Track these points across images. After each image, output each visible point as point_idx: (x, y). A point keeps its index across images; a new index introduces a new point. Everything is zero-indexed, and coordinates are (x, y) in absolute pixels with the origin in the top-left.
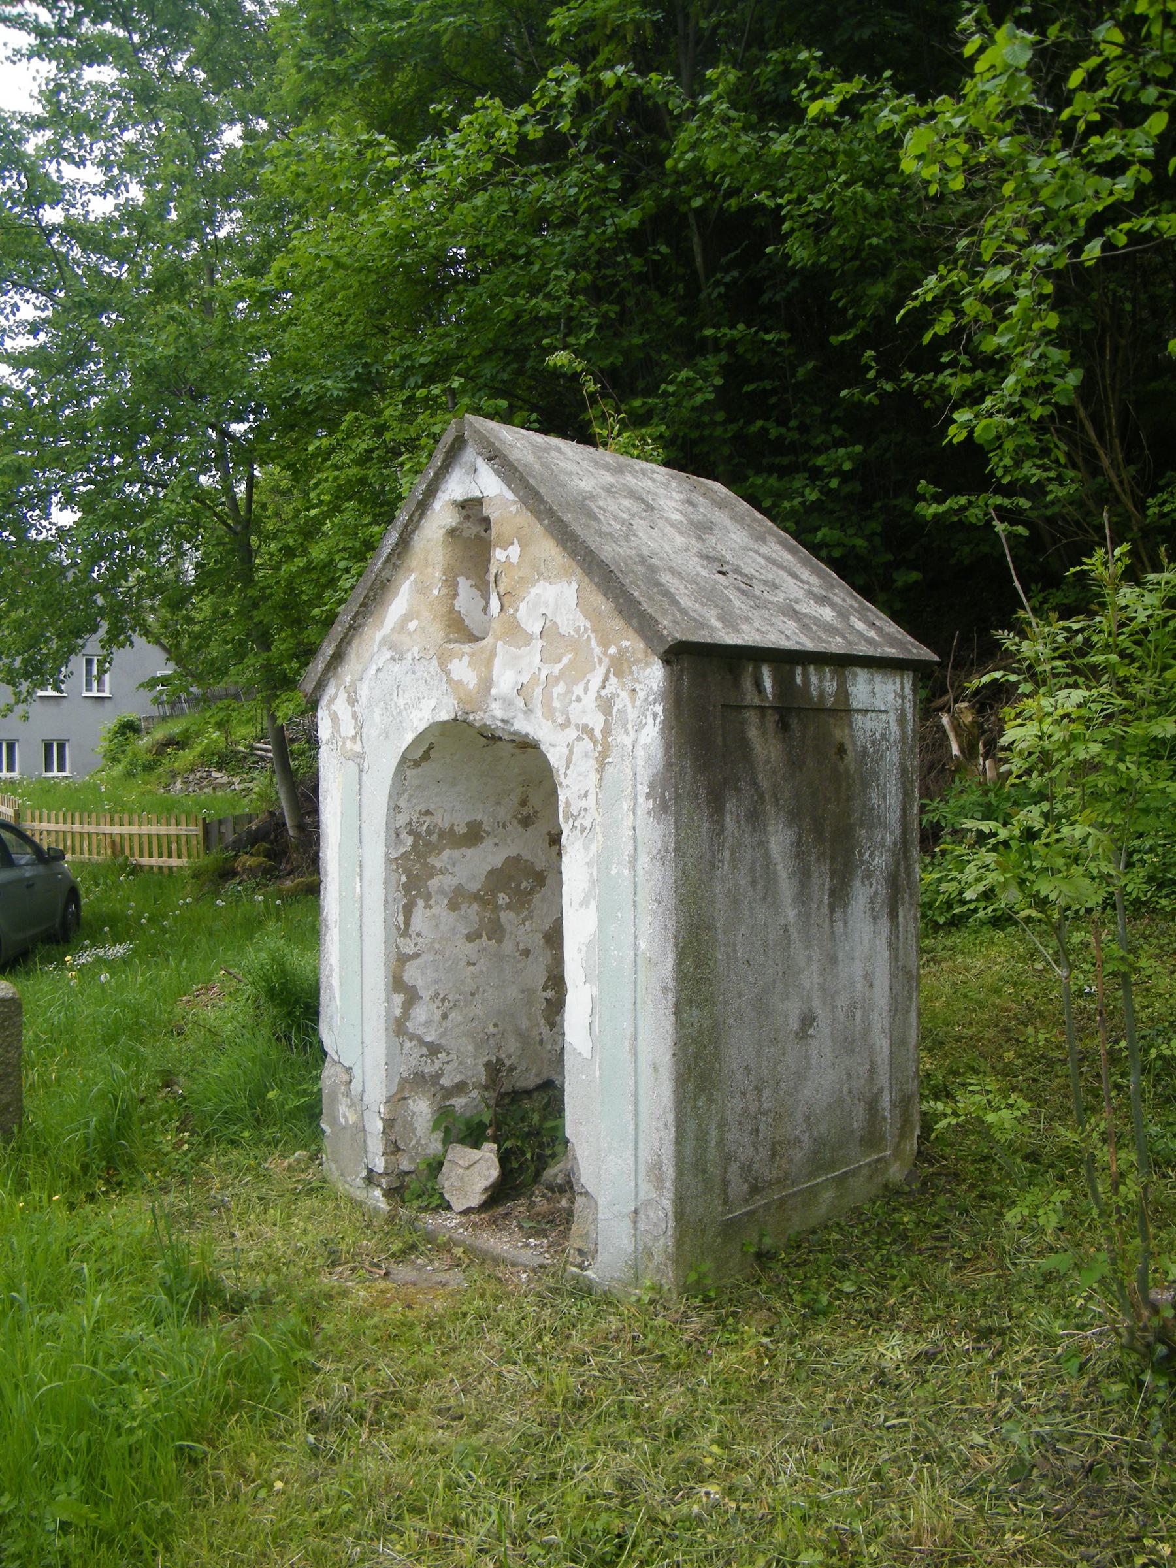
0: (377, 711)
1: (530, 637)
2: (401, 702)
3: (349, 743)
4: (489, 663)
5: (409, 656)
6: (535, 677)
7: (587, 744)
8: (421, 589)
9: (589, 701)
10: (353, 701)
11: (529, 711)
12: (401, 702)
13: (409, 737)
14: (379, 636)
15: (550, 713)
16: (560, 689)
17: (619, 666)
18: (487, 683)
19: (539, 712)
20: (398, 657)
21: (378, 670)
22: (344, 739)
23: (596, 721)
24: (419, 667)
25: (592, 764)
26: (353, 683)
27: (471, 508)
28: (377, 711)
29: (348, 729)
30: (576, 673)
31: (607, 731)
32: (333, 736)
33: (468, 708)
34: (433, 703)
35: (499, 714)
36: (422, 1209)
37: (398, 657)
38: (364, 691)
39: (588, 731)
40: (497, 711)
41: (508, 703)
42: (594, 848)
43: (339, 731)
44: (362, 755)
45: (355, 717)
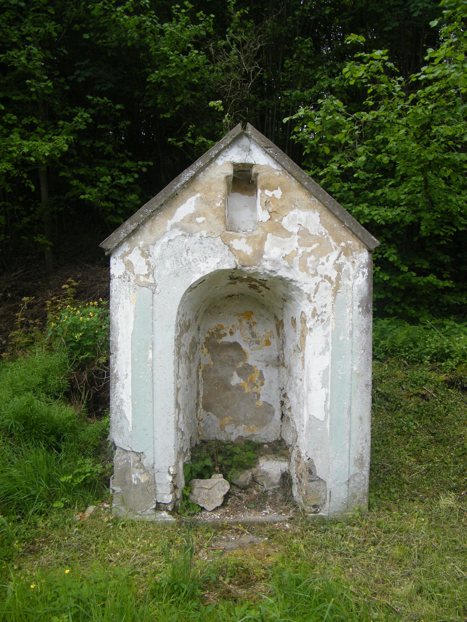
0: (168, 264)
1: (290, 234)
9: (330, 265)
21: (170, 240)
22: (138, 276)
23: (333, 275)
24: (206, 242)
26: (146, 246)
30: (323, 251)
33: (246, 263)
38: (156, 251)
40: (268, 266)
42: (330, 329)
44: (155, 285)
45: (148, 264)
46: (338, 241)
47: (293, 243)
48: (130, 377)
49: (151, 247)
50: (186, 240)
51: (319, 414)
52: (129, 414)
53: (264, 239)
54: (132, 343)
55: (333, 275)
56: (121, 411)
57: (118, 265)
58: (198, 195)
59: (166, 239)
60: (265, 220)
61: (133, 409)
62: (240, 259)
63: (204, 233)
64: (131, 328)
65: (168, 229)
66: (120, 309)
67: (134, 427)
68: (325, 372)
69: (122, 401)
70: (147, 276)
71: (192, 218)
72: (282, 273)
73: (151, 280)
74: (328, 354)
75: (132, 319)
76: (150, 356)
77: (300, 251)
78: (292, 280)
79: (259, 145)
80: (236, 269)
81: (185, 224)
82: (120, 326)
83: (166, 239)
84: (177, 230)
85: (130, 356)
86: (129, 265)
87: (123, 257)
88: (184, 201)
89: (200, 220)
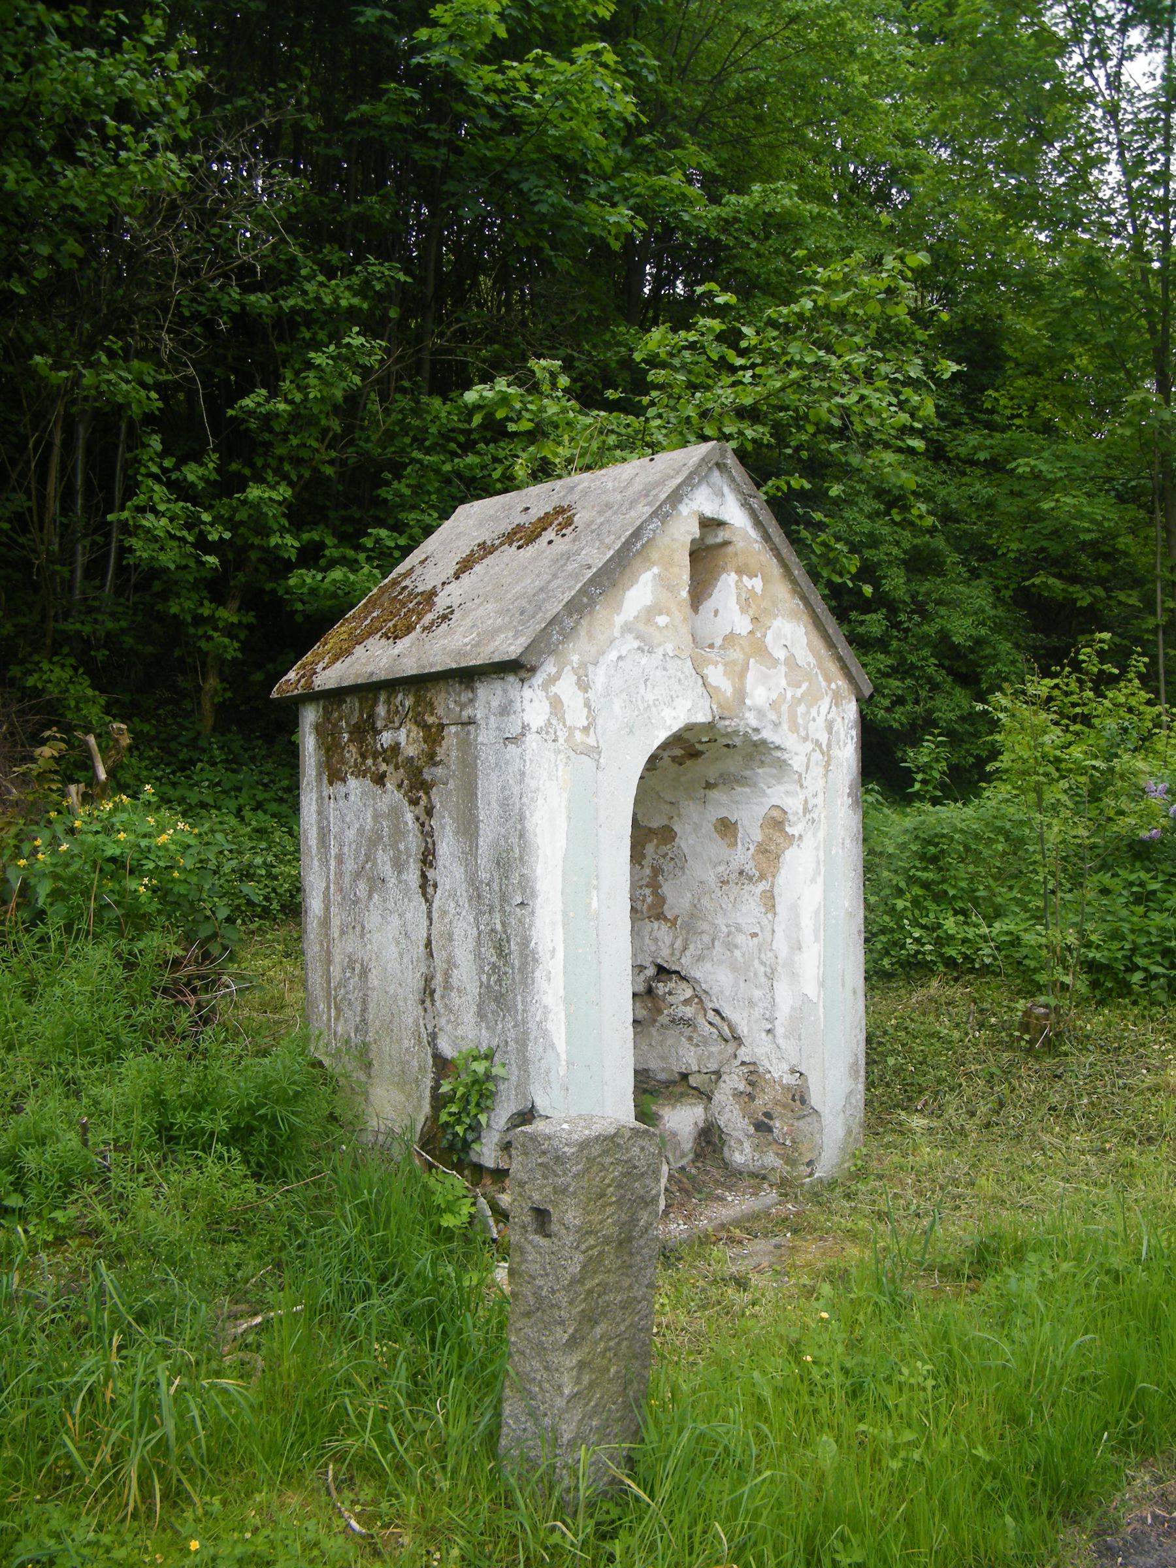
0: (617, 706)
1: (777, 661)
2: (650, 697)
3: (579, 736)
4: (742, 674)
5: (660, 651)
6: (782, 697)
7: (817, 756)
8: (665, 583)
9: (821, 721)
10: (583, 685)
11: (777, 725)
12: (650, 697)
13: (661, 736)
14: (619, 620)
15: (794, 727)
16: (801, 709)
17: (837, 699)
18: (741, 694)
19: (785, 726)
20: (647, 648)
21: (620, 658)
22: (571, 730)
23: (823, 738)
24: (672, 665)
25: (821, 770)
26: (583, 665)
27: (709, 524)
28: (617, 706)
29: (576, 716)
30: (811, 699)
31: (829, 746)
32: (549, 723)
33: (726, 714)
34: (689, 705)
35: (754, 723)
36: (82, 215)
37: (647, 648)
38: (599, 677)
39: (818, 744)
40: (752, 720)
41: (760, 713)
42: (821, 834)
43: (562, 720)
44: (597, 750)
45: (587, 705)
46: (829, 681)
47: (780, 677)
48: (560, 954)
49: (591, 668)
50: (644, 661)
51: (811, 988)
52: (559, 1036)
53: (745, 668)
54: (565, 879)
55: (823, 738)
56: (545, 1034)
57: (536, 703)
58: (655, 570)
59: (613, 655)
60: (744, 633)
61: (569, 1024)
62: (720, 706)
63: (669, 648)
64: (562, 843)
65: (617, 633)
66: (540, 802)
67: (570, 1063)
68: (817, 913)
69: (546, 1010)
70: (586, 729)
71: (651, 612)
72: (767, 734)
73: (591, 741)
74: (820, 880)
75: (564, 826)
76: (595, 904)
77: (789, 695)
78: (778, 748)
79: (738, 490)
80: (711, 726)
81: (641, 627)
82: (539, 840)
83: (613, 655)
84: (629, 637)
85: (559, 906)
86: (556, 704)
87: (546, 686)
88: (634, 581)
89: (662, 620)
